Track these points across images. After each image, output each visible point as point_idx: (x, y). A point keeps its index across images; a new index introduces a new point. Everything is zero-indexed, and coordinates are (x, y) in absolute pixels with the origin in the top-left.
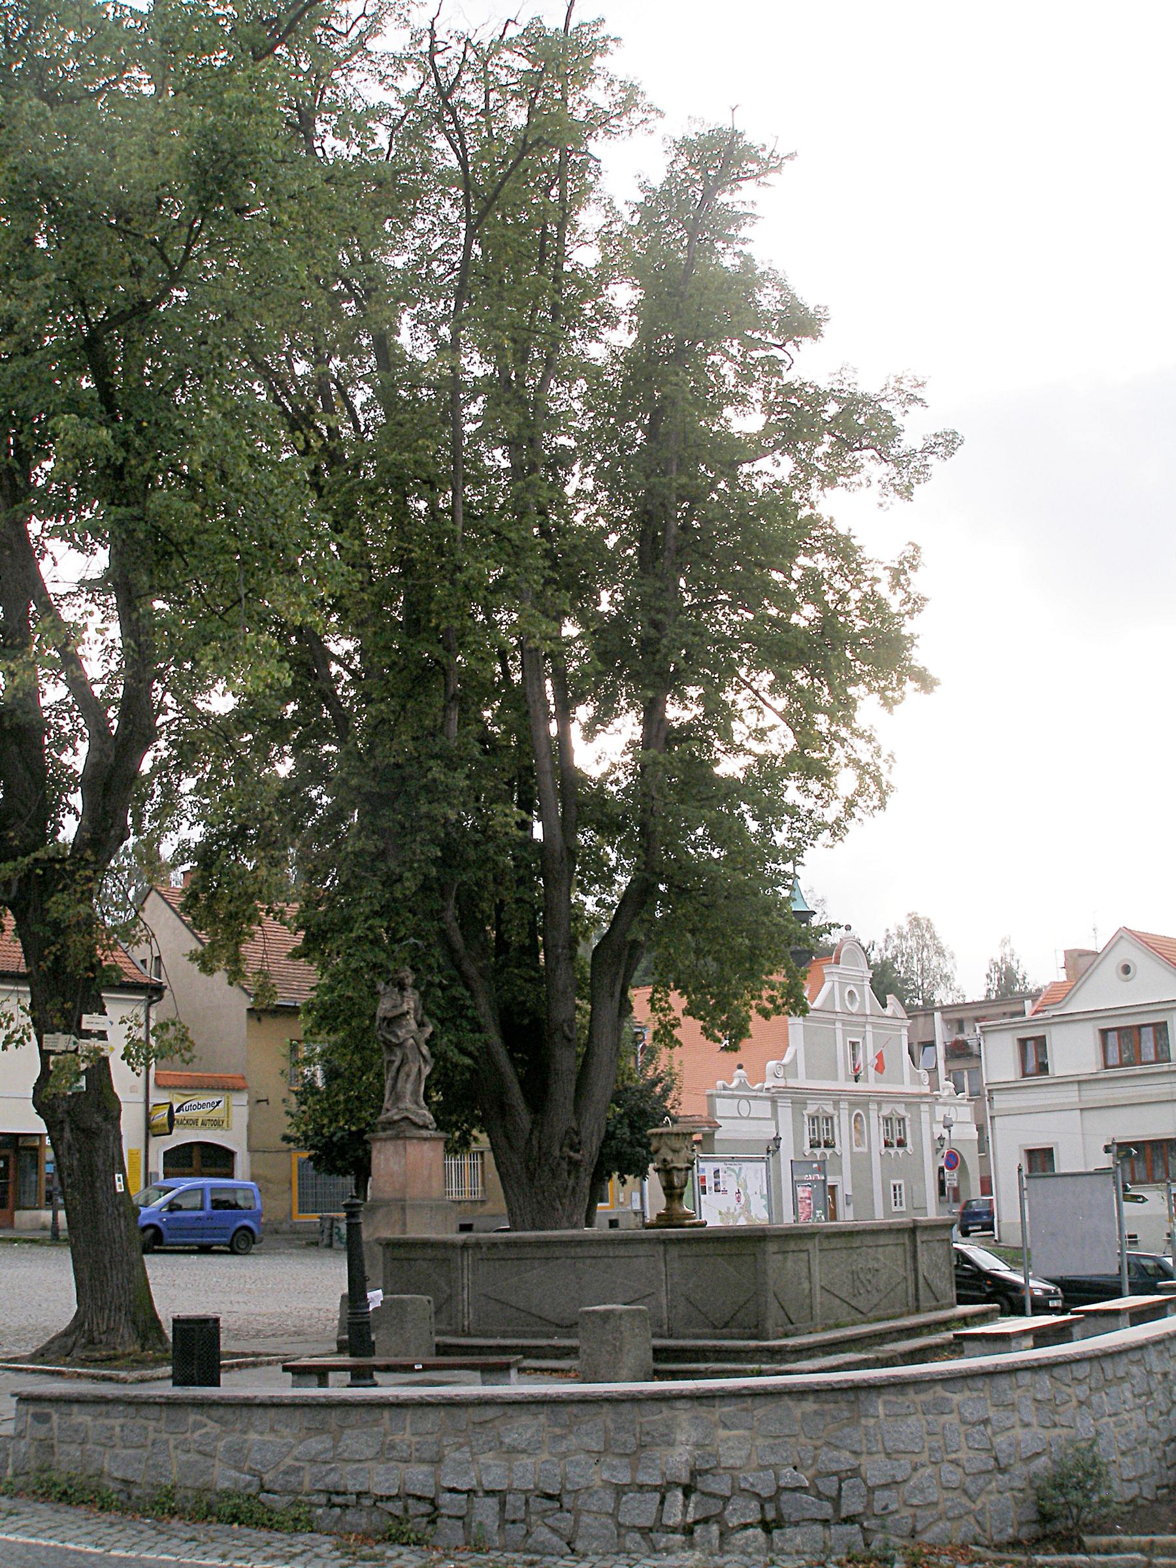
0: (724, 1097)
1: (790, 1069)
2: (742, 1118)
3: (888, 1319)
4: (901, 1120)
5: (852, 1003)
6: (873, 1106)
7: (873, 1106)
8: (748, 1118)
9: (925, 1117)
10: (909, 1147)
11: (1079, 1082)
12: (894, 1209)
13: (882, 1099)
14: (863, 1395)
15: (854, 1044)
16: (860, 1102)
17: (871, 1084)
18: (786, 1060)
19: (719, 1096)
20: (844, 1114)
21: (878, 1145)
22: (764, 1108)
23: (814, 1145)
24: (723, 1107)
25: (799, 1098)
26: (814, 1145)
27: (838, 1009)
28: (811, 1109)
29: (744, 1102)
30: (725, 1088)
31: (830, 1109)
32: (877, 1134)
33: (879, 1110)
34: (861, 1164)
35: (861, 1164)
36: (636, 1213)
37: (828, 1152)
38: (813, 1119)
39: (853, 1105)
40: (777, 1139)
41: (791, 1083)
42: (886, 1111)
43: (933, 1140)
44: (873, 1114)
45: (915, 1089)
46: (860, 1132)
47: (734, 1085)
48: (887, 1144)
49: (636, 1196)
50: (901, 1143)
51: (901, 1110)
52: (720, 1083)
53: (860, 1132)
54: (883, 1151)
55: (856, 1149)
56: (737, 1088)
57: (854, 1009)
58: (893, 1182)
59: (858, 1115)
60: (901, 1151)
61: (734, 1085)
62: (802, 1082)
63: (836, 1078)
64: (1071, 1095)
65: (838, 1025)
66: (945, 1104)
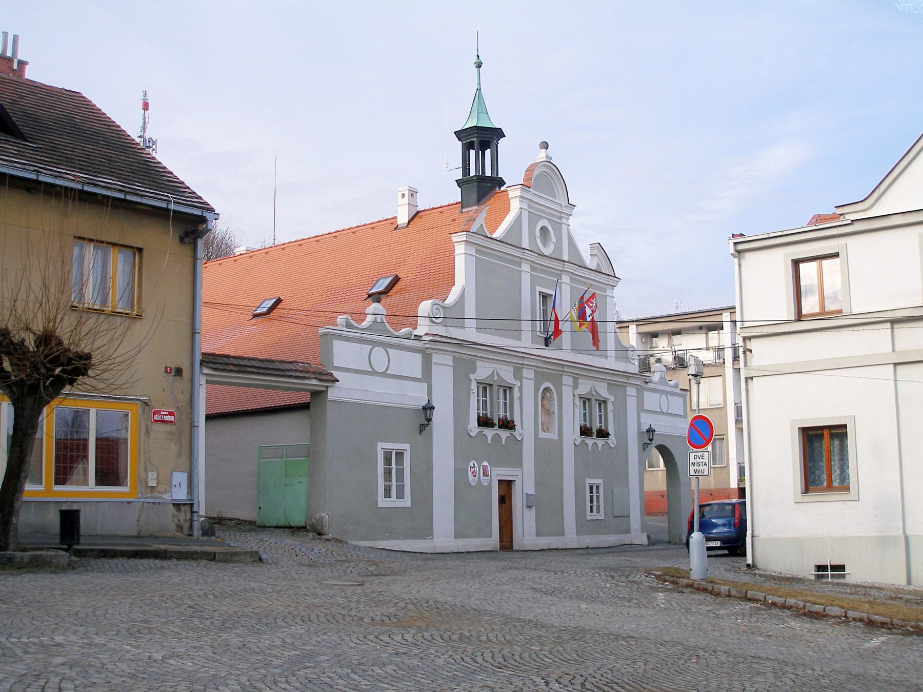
0: (349, 339)
1: (454, 316)
2: (374, 373)
3: (35, 550)
4: (603, 403)
5: (545, 244)
6: (567, 380)
7: (567, 380)
8: (385, 374)
9: (631, 403)
10: (612, 440)
11: (894, 322)
12: (589, 516)
13: (582, 371)
14: (85, 242)
15: (545, 297)
16: (551, 375)
17: (563, 352)
18: (451, 299)
19: (339, 337)
20: (529, 387)
21: (571, 434)
22: (412, 364)
23: (484, 422)
24: (345, 355)
25: (465, 354)
26: (484, 422)
27: (525, 245)
28: (483, 371)
29: (378, 350)
30: (348, 325)
31: (507, 374)
32: (571, 419)
33: (575, 386)
34: (548, 454)
35: (548, 454)
36: (177, 506)
37: (504, 434)
38: (485, 387)
39: (541, 376)
40: (428, 408)
41: (455, 333)
42: (585, 388)
43: (640, 433)
44: (567, 393)
45: (621, 366)
46: (548, 412)
47: (365, 324)
48: (585, 432)
49: (180, 478)
50: (602, 434)
51: (604, 392)
52: (341, 319)
53: (548, 412)
54: (579, 440)
55: (542, 435)
56: (368, 329)
57: (548, 251)
58: (589, 481)
59: (547, 390)
60: (600, 442)
61: (365, 324)
62: (469, 333)
63: (517, 333)
64: (877, 340)
65: (525, 267)
66: (655, 391)
